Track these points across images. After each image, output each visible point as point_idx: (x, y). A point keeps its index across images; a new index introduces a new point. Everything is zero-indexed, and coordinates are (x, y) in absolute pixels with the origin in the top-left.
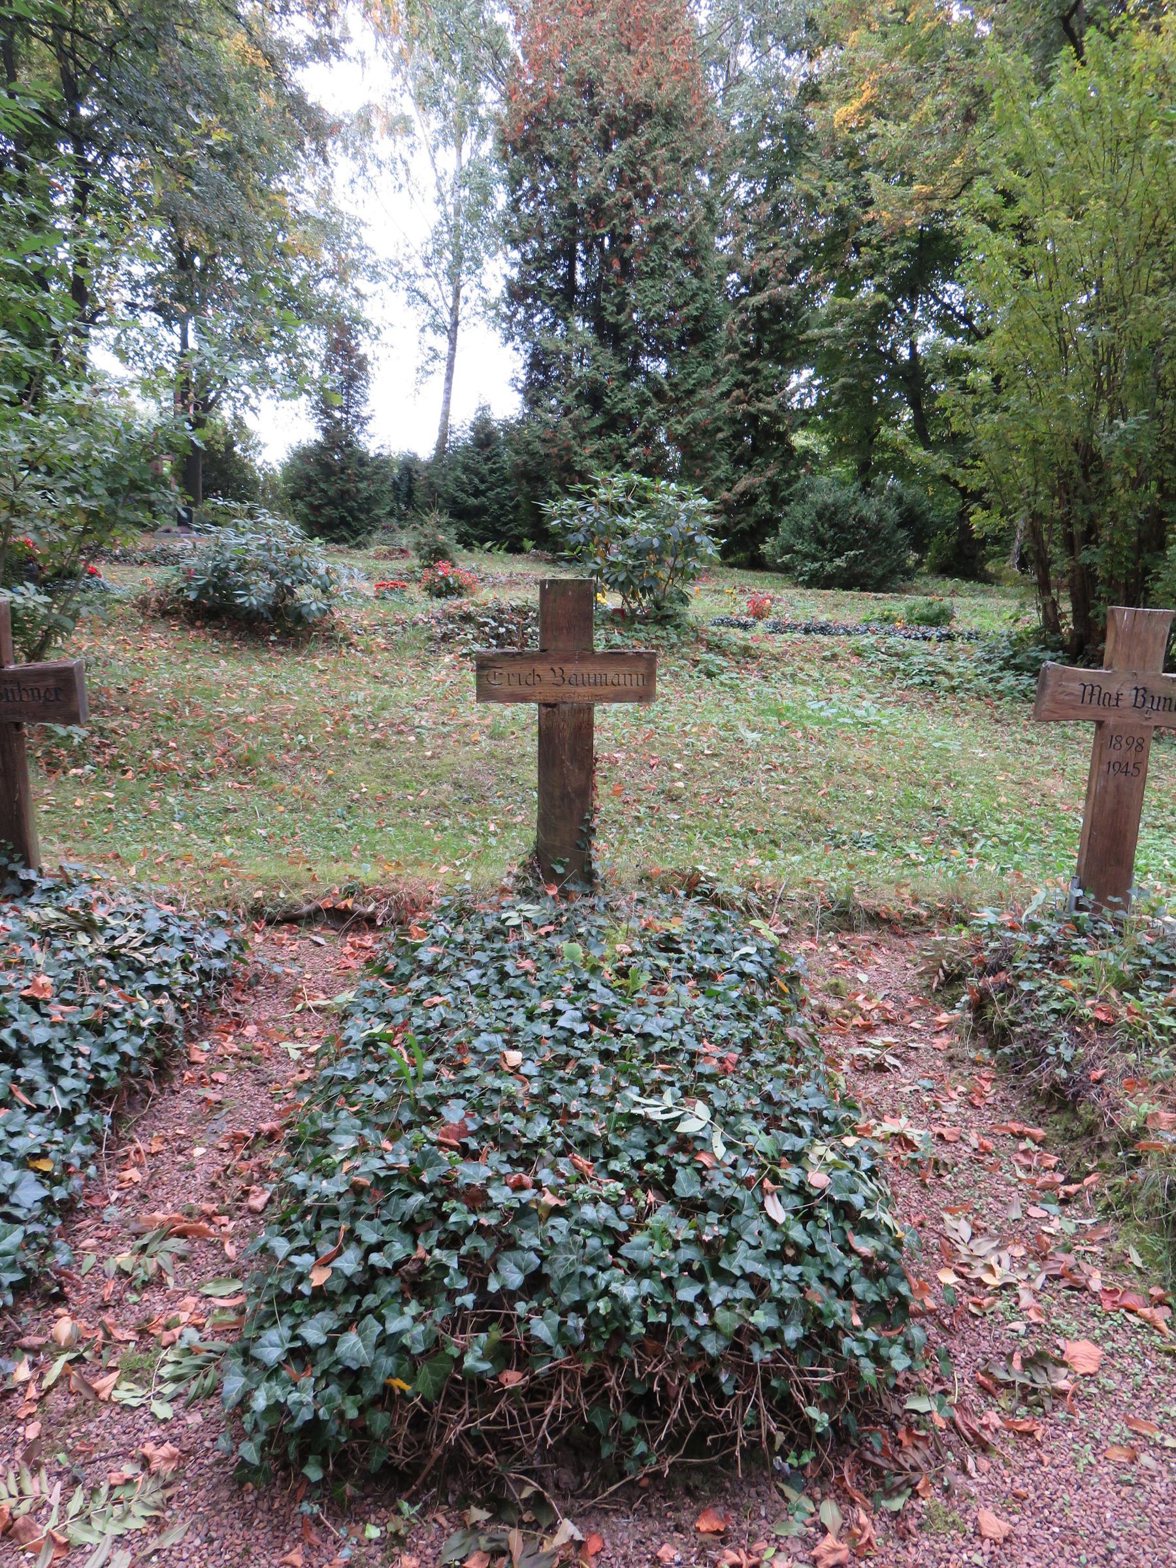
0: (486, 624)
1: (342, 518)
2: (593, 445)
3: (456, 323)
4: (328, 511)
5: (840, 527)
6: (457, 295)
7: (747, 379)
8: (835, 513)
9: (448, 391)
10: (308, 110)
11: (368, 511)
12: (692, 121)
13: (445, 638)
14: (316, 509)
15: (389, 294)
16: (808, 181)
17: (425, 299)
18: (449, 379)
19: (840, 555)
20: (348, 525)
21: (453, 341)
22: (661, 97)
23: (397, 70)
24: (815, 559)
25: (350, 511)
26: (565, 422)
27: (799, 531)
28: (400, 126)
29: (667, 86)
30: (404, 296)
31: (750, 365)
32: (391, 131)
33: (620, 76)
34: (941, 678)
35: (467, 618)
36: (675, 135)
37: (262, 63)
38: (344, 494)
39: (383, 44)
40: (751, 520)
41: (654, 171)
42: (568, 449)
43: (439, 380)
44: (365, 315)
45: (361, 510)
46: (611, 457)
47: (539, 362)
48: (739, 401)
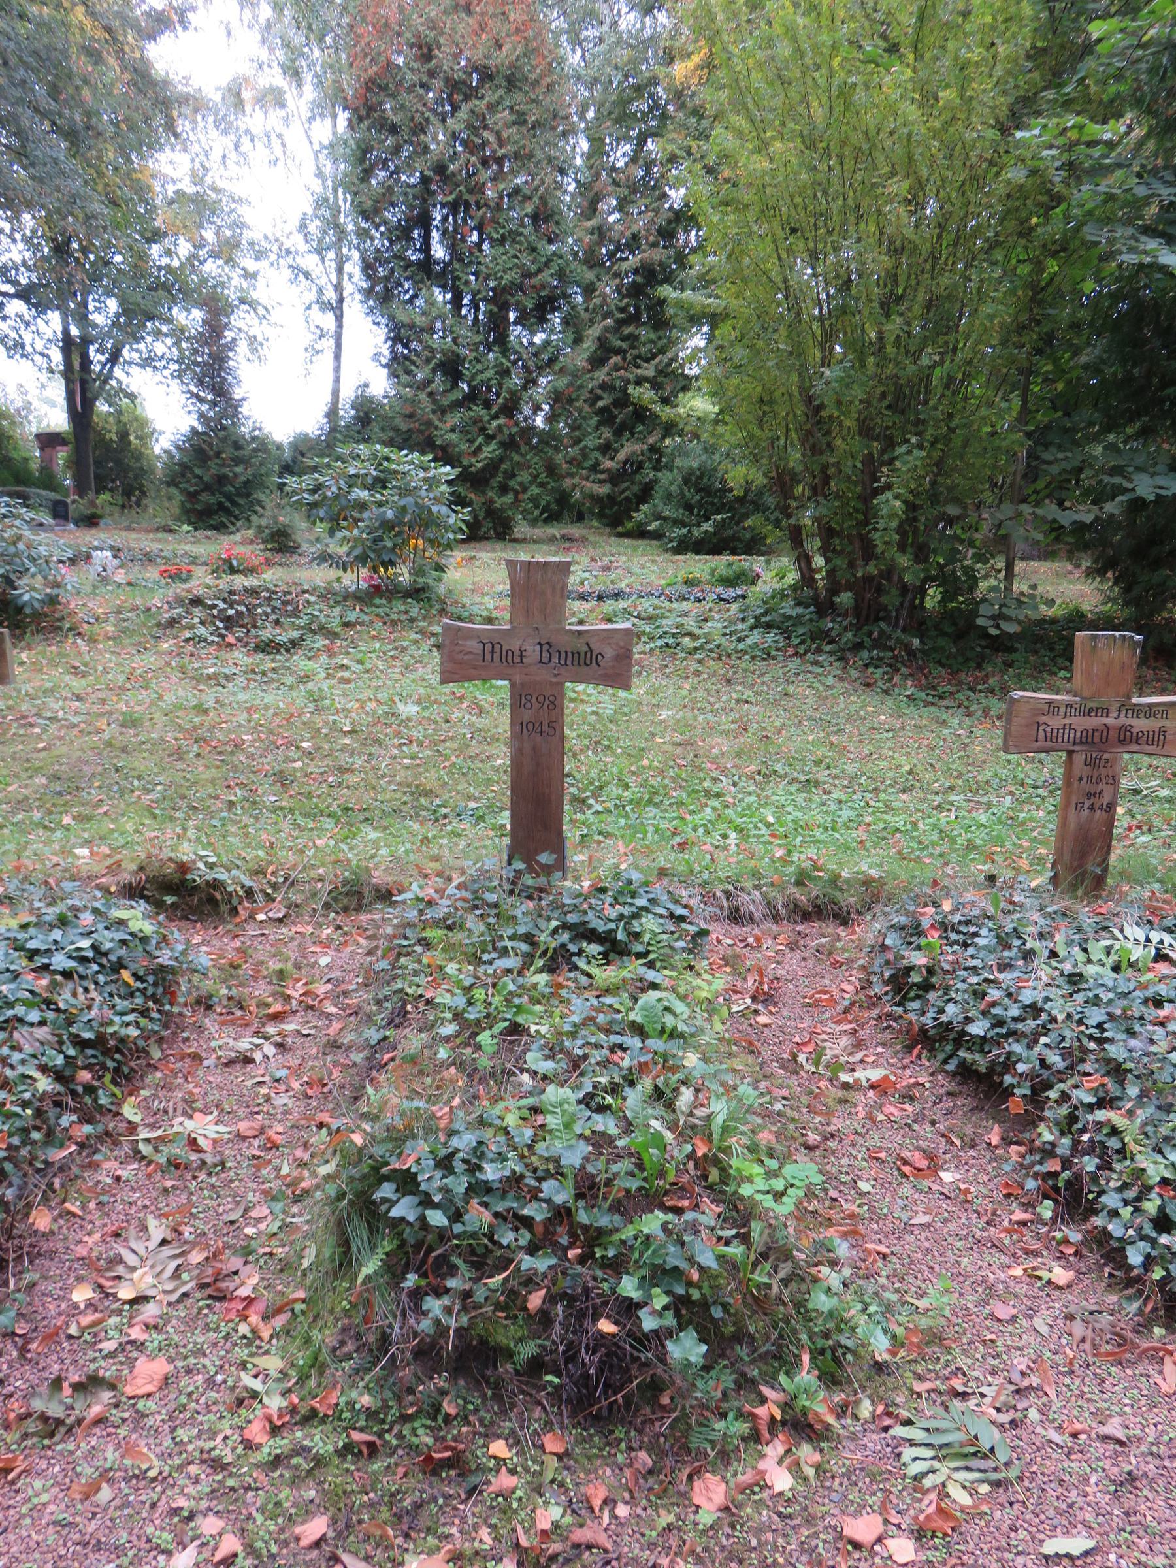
0: (215, 606)
1: (220, 504)
2: (455, 419)
3: (341, 300)
4: (205, 497)
5: (706, 491)
6: (340, 271)
7: (624, 345)
8: (700, 477)
9: (337, 369)
10: (153, 83)
11: (248, 495)
12: (536, 83)
13: (172, 622)
14: (192, 496)
15: (272, 272)
16: (672, 141)
17: (307, 275)
18: (337, 357)
19: (707, 519)
20: (228, 512)
21: (339, 318)
22: (500, 59)
23: (264, 41)
24: (683, 524)
25: (229, 497)
26: (423, 396)
27: (669, 496)
28: (274, 98)
29: (506, 47)
30: (287, 273)
31: (627, 330)
32: (260, 100)
33: (457, 37)
34: (687, 640)
35: (197, 601)
36: (518, 97)
37: (100, 34)
38: (221, 480)
39: (247, 14)
40: (636, 488)
41: (498, 135)
42: (429, 423)
43: (329, 356)
44: (255, 295)
45: (239, 495)
46: (474, 430)
47: (399, 335)
48: (617, 368)
